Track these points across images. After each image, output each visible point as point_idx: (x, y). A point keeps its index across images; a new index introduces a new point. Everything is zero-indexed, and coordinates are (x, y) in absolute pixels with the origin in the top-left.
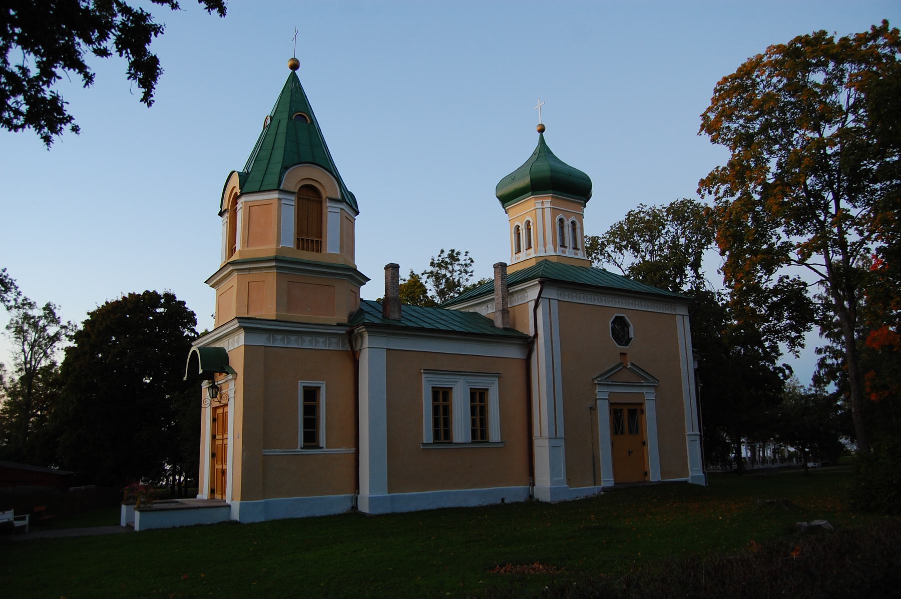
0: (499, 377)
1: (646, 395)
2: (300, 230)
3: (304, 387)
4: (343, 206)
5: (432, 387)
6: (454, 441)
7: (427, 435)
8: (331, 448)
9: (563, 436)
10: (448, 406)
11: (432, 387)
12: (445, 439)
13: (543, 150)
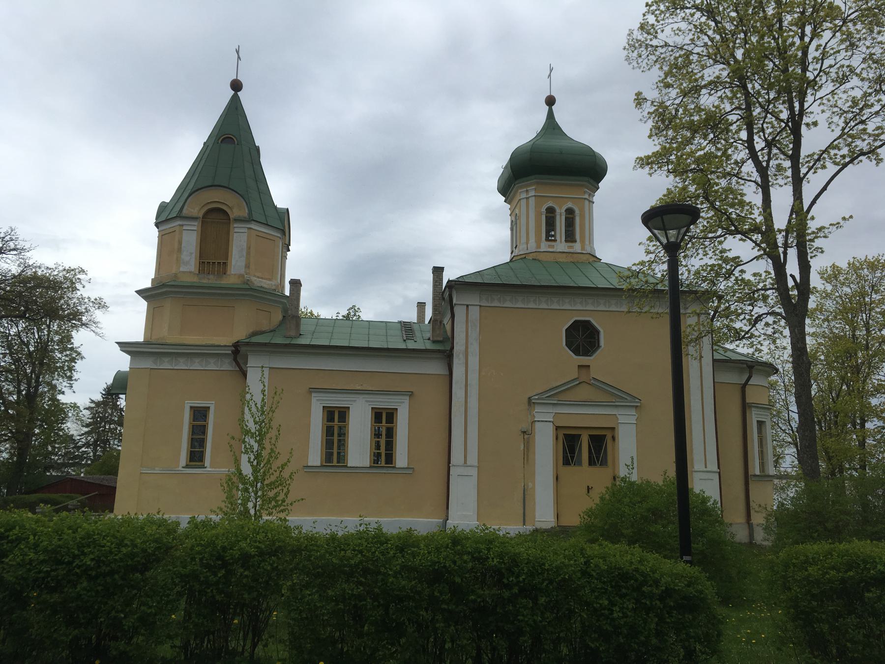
0: (410, 396)
1: (618, 416)
2: (202, 254)
3: (191, 407)
4: (253, 226)
5: (324, 407)
6: (349, 465)
7: (315, 458)
8: (215, 468)
9: (476, 464)
10: (393, 428)
11: (324, 407)
12: (386, 464)
13: (551, 126)
